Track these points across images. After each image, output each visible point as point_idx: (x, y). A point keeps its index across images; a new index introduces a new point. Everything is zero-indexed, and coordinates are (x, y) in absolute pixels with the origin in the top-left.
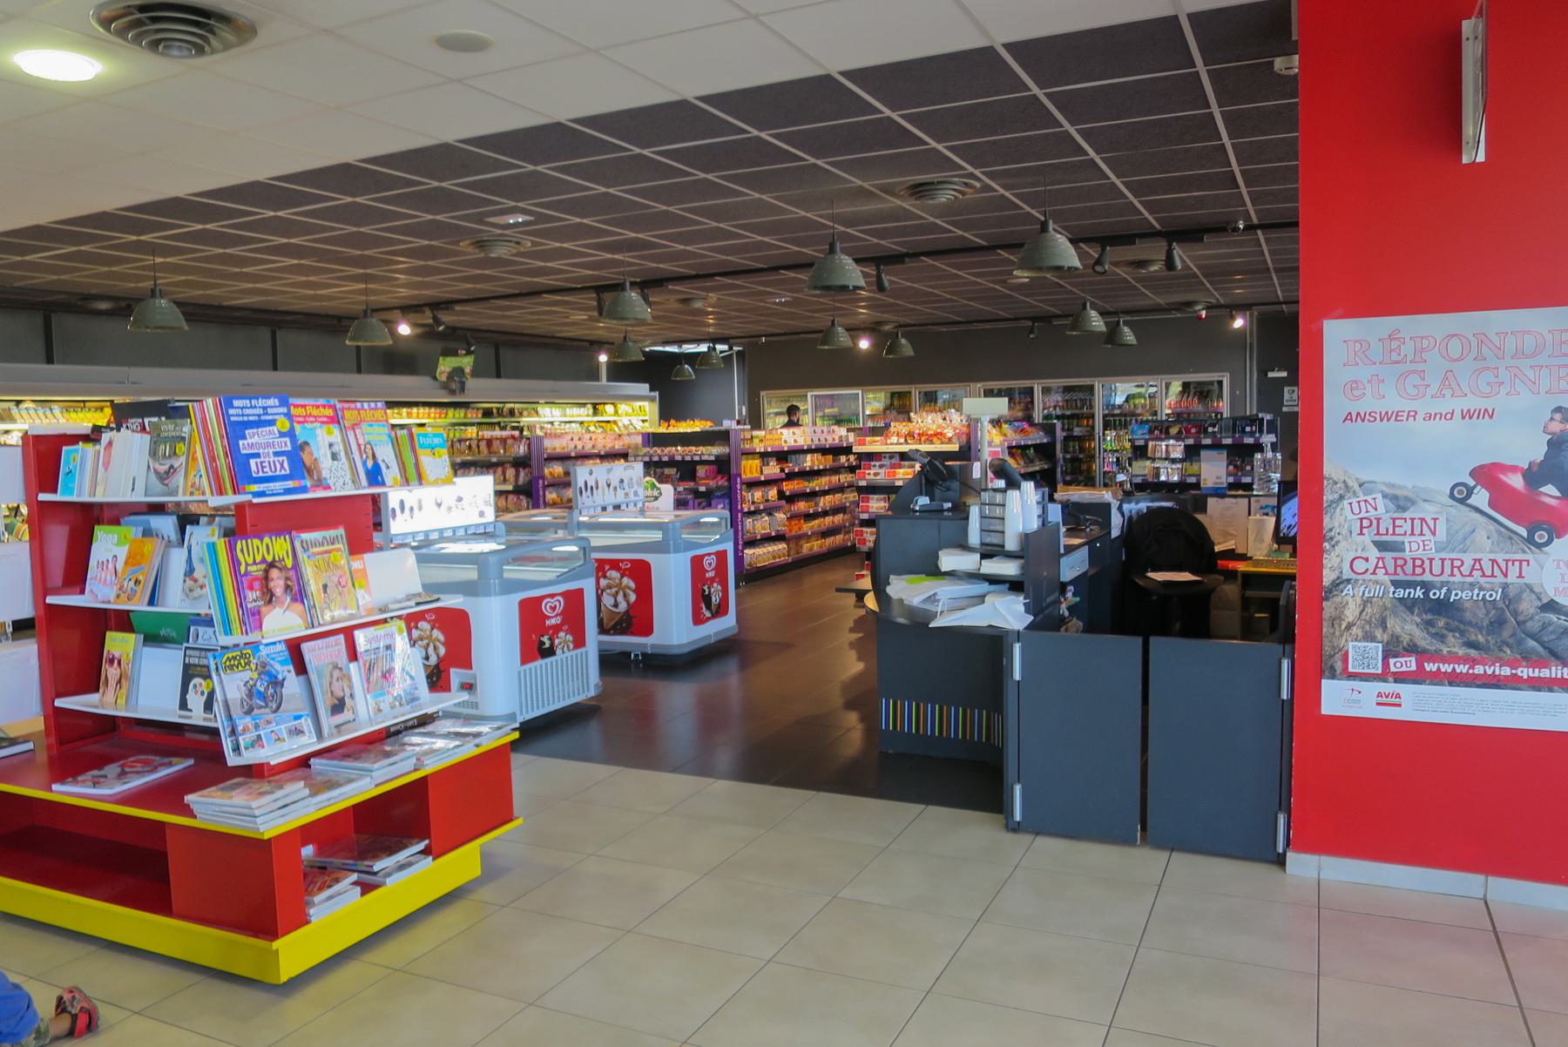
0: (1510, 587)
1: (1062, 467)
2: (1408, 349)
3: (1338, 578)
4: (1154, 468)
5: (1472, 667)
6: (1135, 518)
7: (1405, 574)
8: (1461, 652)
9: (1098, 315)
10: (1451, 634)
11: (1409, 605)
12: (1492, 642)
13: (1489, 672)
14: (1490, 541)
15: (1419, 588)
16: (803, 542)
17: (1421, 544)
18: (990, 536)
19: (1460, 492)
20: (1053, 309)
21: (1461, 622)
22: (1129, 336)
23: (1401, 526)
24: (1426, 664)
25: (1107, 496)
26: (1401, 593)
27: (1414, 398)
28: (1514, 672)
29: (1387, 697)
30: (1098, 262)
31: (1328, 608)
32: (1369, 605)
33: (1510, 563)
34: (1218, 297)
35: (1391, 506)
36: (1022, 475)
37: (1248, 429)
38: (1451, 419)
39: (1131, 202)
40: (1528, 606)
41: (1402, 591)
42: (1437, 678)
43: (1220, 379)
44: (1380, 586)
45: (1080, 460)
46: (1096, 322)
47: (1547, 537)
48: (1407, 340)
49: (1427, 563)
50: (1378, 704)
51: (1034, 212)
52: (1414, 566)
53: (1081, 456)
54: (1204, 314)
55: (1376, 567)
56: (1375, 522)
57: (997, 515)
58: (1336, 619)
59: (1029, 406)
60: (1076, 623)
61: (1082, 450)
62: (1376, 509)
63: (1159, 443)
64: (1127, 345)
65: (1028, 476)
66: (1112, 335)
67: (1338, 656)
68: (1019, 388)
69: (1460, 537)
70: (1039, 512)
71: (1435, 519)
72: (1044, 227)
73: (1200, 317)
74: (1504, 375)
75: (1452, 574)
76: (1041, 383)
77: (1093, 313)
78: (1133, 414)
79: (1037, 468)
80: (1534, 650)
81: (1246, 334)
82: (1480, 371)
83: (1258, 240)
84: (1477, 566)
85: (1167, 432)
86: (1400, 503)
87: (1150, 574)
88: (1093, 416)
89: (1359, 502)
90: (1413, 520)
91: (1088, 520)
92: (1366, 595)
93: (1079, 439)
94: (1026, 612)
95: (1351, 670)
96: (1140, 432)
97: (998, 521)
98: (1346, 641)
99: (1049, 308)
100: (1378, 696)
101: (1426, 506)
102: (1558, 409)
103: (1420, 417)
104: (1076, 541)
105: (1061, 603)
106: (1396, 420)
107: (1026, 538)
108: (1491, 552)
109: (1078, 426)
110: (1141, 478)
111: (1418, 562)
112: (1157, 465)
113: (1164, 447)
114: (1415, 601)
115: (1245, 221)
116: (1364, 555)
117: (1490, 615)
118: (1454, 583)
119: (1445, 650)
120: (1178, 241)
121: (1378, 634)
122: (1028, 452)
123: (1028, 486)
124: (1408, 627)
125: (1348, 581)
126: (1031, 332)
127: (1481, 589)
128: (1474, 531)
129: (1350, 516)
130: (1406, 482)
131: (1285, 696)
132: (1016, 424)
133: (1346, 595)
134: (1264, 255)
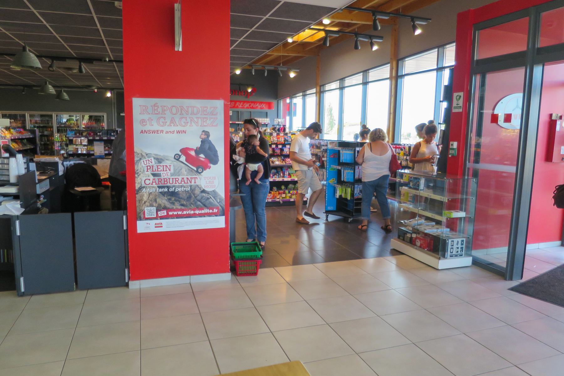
0: (192, 186)
1: (40, 147)
2: (160, 110)
3: (141, 186)
4: (76, 148)
5: (183, 212)
6: (69, 167)
7: (162, 184)
8: (179, 207)
9: (52, 87)
10: (176, 202)
11: (163, 194)
12: (188, 204)
13: (188, 213)
14: (186, 172)
15: (166, 188)
16: (422, 177)
17: (166, 174)
18: (3, 177)
19: (177, 157)
20: (8, 82)
21: (179, 198)
22: (66, 96)
23: (160, 168)
24: (169, 213)
25: (56, 159)
26: (161, 190)
27: (162, 126)
28: (194, 212)
29: (158, 224)
30: (51, 66)
31: (138, 197)
32: (151, 195)
33: (192, 179)
34: (101, 85)
35: (156, 161)
36: (17, 151)
37: (112, 134)
38: (174, 133)
39: (63, 45)
40: (197, 192)
41: (161, 189)
42: (173, 217)
43: (103, 115)
44: (154, 189)
45: (48, 145)
46: (51, 90)
47: (202, 170)
48: (160, 107)
49: (168, 180)
50: (156, 227)
51: (20, 42)
52: (164, 181)
53: (48, 143)
54: (96, 90)
55: (153, 182)
56: (152, 167)
57: (6, 168)
58: (140, 201)
59: (24, 122)
60: (46, 210)
61: (48, 140)
62: (152, 163)
63: (78, 139)
64: (65, 100)
65: (19, 152)
66: (59, 95)
67: (142, 213)
68: (20, 115)
69: (177, 171)
70: (26, 166)
71: (170, 166)
72: (24, 49)
73: (94, 92)
74: (189, 120)
75: (176, 183)
76: (82, 114)
77: (50, 86)
78: (69, 127)
79: (29, 148)
80: (199, 205)
81: (112, 101)
82: (181, 118)
83: (114, 66)
84: (183, 180)
85: (82, 134)
86: (159, 160)
87: (76, 189)
88: (52, 127)
89: (146, 161)
90: (163, 166)
91: (49, 169)
92: (150, 191)
93: (47, 136)
94: (21, 207)
95: (146, 217)
96: (71, 134)
97: (6, 171)
98: (144, 207)
99: (31, 82)
100: (155, 225)
101: (167, 161)
102: (204, 131)
103: (164, 132)
104: (44, 177)
105: (37, 202)
106: (157, 133)
107: (19, 177)
108: (186, 175)
109: (46, 131)
110: (72, 152)
111: (166, 180)
112: (77, 147)
113: (79, 140)
114: (165, 192)
115: (109, 58)
116: (149, 178)
117: (187, 195)
118: (176, 186)
119: (175, 207)
120: (84, 62)
121: (154, 204)
122: (23, 141)
123: (20, 156)
124: (163, 201)
125: (144, 187)
126: (23, 91)
127: (184, 187)
128: (181, 169)
129: (144, 165)
130: (161, 153)
131: (125, 228)
132: (18, 129)
133: (144, 192)
134: (116, 71)
